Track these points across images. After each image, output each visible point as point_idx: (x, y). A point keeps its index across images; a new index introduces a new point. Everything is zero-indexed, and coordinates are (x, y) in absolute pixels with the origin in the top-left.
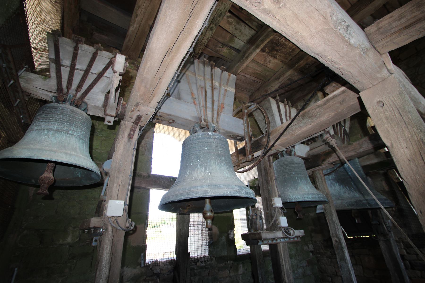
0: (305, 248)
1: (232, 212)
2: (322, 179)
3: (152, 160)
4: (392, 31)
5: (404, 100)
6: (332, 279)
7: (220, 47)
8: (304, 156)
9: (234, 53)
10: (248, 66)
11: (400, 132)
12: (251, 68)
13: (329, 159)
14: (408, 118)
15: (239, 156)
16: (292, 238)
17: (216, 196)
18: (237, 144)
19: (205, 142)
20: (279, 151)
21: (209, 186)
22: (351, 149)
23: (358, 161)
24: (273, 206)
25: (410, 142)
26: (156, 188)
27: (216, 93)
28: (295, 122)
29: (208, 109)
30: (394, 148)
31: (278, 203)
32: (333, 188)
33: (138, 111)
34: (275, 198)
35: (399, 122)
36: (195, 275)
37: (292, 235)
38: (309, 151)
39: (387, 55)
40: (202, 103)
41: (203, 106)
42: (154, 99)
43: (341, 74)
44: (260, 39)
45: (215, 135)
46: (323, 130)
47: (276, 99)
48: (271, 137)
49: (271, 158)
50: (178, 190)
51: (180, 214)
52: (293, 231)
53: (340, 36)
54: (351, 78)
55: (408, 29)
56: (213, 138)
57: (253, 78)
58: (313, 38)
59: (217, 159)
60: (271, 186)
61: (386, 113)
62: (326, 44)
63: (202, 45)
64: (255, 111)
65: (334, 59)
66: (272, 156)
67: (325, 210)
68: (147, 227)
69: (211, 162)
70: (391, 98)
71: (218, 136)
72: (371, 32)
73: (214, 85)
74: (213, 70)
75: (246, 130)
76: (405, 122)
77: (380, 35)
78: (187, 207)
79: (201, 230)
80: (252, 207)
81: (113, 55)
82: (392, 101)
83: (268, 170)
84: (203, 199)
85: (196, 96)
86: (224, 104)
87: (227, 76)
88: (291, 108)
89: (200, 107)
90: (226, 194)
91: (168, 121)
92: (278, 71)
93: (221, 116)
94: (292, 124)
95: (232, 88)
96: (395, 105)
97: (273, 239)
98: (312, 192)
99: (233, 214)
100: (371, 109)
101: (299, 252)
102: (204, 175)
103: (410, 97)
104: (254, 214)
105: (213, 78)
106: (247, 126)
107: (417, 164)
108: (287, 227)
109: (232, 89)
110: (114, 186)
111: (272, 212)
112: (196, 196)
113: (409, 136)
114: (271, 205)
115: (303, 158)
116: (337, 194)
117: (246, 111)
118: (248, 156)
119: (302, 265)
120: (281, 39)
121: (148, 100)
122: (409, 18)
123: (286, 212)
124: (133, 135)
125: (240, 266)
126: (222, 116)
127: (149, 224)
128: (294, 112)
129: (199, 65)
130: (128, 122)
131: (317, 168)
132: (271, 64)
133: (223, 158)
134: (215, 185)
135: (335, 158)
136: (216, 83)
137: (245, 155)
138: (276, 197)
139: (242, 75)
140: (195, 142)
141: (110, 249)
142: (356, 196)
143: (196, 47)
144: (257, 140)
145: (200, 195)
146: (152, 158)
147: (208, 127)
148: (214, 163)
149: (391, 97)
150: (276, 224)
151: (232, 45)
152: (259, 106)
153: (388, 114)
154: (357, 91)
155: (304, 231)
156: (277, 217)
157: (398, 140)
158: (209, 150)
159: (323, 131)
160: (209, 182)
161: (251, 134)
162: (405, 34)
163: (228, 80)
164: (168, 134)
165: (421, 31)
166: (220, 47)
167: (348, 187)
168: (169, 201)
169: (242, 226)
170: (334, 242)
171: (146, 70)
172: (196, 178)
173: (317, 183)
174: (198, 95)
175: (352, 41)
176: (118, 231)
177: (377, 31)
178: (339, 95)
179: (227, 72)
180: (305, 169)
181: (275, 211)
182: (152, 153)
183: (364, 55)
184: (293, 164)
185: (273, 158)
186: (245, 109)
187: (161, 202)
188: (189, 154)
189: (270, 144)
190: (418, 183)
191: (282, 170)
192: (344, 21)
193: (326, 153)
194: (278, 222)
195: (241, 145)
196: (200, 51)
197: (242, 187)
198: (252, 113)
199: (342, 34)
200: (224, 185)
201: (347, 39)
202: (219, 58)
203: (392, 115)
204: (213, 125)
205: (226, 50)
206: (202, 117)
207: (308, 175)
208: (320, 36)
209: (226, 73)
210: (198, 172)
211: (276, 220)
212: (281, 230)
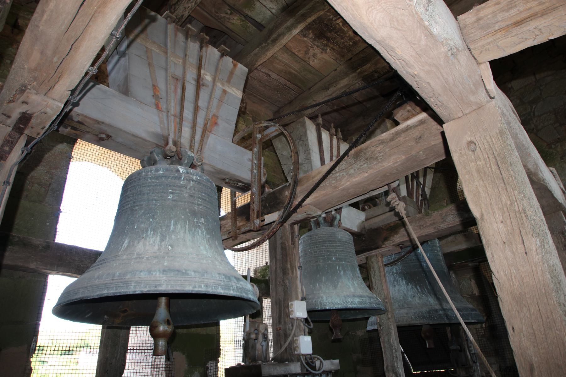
1: (218, 325)
2: (380, 272)
3: (59, 214)
4: (497, 27)
5: (505, 144)
7: (227, 13)
8: (355, 229)
9: (252, 28)
10: (275, 58)
11: (495, 195)
12: (280, 61)
13: (394, 237)
14: (509, 173)
15: (239, 219)
16: (318, 374)
17: (177, 292)
18: (235, 196)
19: (170, 186)
22: (428, 224)
23: (438, 245)
24: (291, 316)
25: (508, 214)
26: (62, 273)
27: (204, 94)
28: (343, 165)
29: (183, 122)
30: (485, 220)
32: (397, 287)
33: (23, 103)
35: (495, 179)
37: (317, 369)
38: (363, 222)
39: (487, 66)
40: (172, 109)
41: (175, 116)
42: (60, 82)
43: (417, 86)
44: (300, 12)
45: (191, 174)
46: (387, 185)
47: (316, 121)
48: (299, 189)
49: (296, 227)
50: (98, 278)
51: (108, 328)
52: (321, 362)
53: (416, 16)
54: (431, 96)
55: (519, 27)
56: (187, 180)
57: (282, 81)
58: (373, 9)
59: (189, 220)
61: (479, 163)
62: (392, 26)
64: (277, 139)
65: (406, 57)
66: (299, 224)
67: (380, 326)
68: (34, 353)
69: (175, 225)
70: (488, 139)
71: (197, 176)
72: (467, 23)
73: (203, 79)
74: (204, 49)
76: (503, 180)
77: (480, 31)
79: (150, 360)
80: (250, 317)
82: (488, 143)
83: (288, 248)
84: (155, 297)
85: (163, 94)
86: (218, 117)
87: (231, 65)
88: (341, 142)
89: (167, 116)
91: (97, 136)
92: (328, 76)
93: (210, 139)
94: (337, 169)
95: (238, 89)
96: (493, 151)
98: (361, 293)
99: (219, 331)
100: (457, 154)
102: (159, 249)
103: (515, 143)
104: (253, 330)
105: (203, 64)
106: (259, 164)
107: (514, 250)
108: (310, 354)
109: (236, 92)
111: (288, 328)
112: (133, 290)
113: (506, 204)
114: (287, 314)
115: (353, 234)
116: (402, 298)
117: (259, 136)
118: (253, 221)
120: (336, 20)
121: (48, 81)
122: (521, 9)
123: (312, 327)
124: (9, 154)
126: (211, 140)
127: (38, 345)
128: (344, 147)
129: (176, 35)
131: (374, 252)
132: (316, 61)
134: (178, 271)
135: (404, 235)
136: (206, 75)
137: (248, 219)
138: (297, 299)
139: (263, 72)
140: (149, 183)
142: (430, 302)
143: (179, 3)
144: (274, 193)
145: (142, 289)
146: (60, 209)
147: (180, 157)
148: (181, 227)
149: (488, 137)
150: (291, 349)
151: (249, 14)
152: (283, 130)
153: (480, 163)
154: (440, 122)
155: (340, 361)
156: (295, 335)
157: (491, 208)
158: (174, 200)
160: (166, 264)
161: (263, 179)
162: (513, 34)
163: (232, 73)
164: (104, 165)
165: (537, 34)
166: (227, 13)
167: (420, 287)
169: (236, 353)
171: (45, 16)
172: (141, 255)
173: (372, 279)
174: (167, 92)
175: (435, 30)
177: (475, 22)
178: (415, 126)
179: (231, 59)
180: (354, 252)
181: (292, 326)
182: (61, 200)
183: (452, 57)
184: (335, 241)
185: (301, 228)
187: (60, 299)
188: (134, 207)
189: (296, 203)
190: (514, 281)
193: (391, 226)
194: (295, 345)
195: (243, 200)
196: (187, 12)
197: (233, 276)
198: (270, 140)
199: (419, 13)
200: (195, 272)
201: (427, 23)
202: (223, 33)
203: (487, 167)
204: (190, 153)
205: (238, 19)
206: (169, 135)
207: (357, 264)
208: (384, 10)
209: (228, 60)
210: (147, 243)
211: (293, 342)
212: (299, 360)
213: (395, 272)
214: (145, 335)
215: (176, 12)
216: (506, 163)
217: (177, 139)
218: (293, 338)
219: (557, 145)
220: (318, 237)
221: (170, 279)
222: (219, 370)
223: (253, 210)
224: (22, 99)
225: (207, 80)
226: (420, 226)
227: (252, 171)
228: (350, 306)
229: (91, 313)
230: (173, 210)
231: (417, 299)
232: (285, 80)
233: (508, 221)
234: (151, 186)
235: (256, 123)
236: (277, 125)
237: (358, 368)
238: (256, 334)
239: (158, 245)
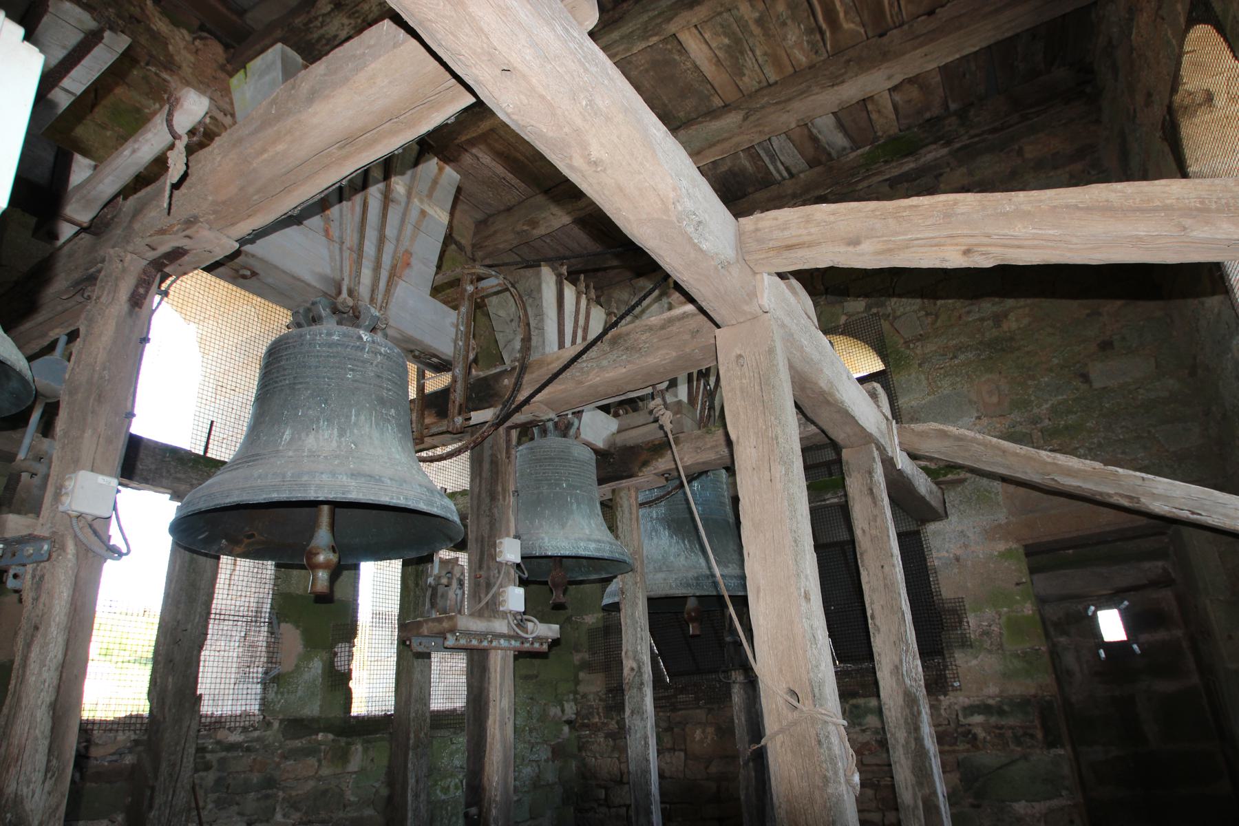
0: (554, 711)
2: (631, 513)
6: (606, 794)
8: (600, 444)
12: (501, 137)
17: (371, 502)
19: (349, 359)
20: (538, 419)
21: (352, 475)
23: (724, 480)
24: (498, 559)
28: (593, 352)
31: (510, 551)
32: (655, 540)
34: (507, 539)
36: (208, 767)
38: (614, 434)
41: (350, 249)
45: (378, 344)
49: (514, 434)
50: (259, 477)
56: (372, 352)
59: (376, 410)
60: (500, 506)
61: (744, 381)
63: (358, 17)
66: (518, 430)
71: (385, 347)
75: (461, 343)
78: (245, 540)
81: (95, 20)
82: (756, 359)
86: (411, 254)
87: (436, 168)
89: (341, 250)
90: (394, 501)
94: (584, 357)
97: (482, 636)
101: (534, 721)
104: (444, 573)
109: (441, 214)
110: (86, 435)
112: (315, 495)
115: (597, 451)
116: (660, 557)
117: (470, 288)
119: (534, 757)
124: (145, 298)
125: (356, 749)
126: (402, 290)
130: (135, 256)
131: (624, 483)
133: (393, 411)
134: (370, 476)
136: (398, 184)
138: (508, 535)
140: (318, 351)
141: (70, 599)
142: (700, 564)
143: (332, 14)
144: (485, 379)
145: (326, 495)
147: (357, 314)
148: (366, 419)
149: (757, 354)
156: (501, 586)
158: (356, 381)
159: (651, 388)
160: (352, 466)
163: (435, 182)
167: (689, 541)
168: (230, 503)
170: (626, 671)
172: (314, 452)
176: (90, 555)
180: (595, 478)
181: (499, 572)
183: (722, 270)
186: (468, 282)
188: (294, 384)
189: (521, 397)
191: (536, 474)
192: (695, 214)
193: (654, 445)
194: (501, 599)
195: (436, 383)
201: (696, 241)
206: (343, 279)
210: (321, 437)
213: (655, 517)
214: (225, 596)
215: (325, 28)
216: (769, 385)
217: (352, 286)
218: (499, 588)
219: (917, 344)
220: (544, 451)
221: (362, 485)
222: (354, 657)
223: (454, 402)
224: (187, 233)
225: (399, 193)
226: (697, 448)
227: (455, 342)
228: (582, 553)
229: (207, 533)
230: (353, 394)
231: (682, 558)
233: (761, 448)
234: (321, 356)
235: (466, 267)
236: (501, 277)
237: (582, 675)
238: (449, 578)
239: (337, 441)
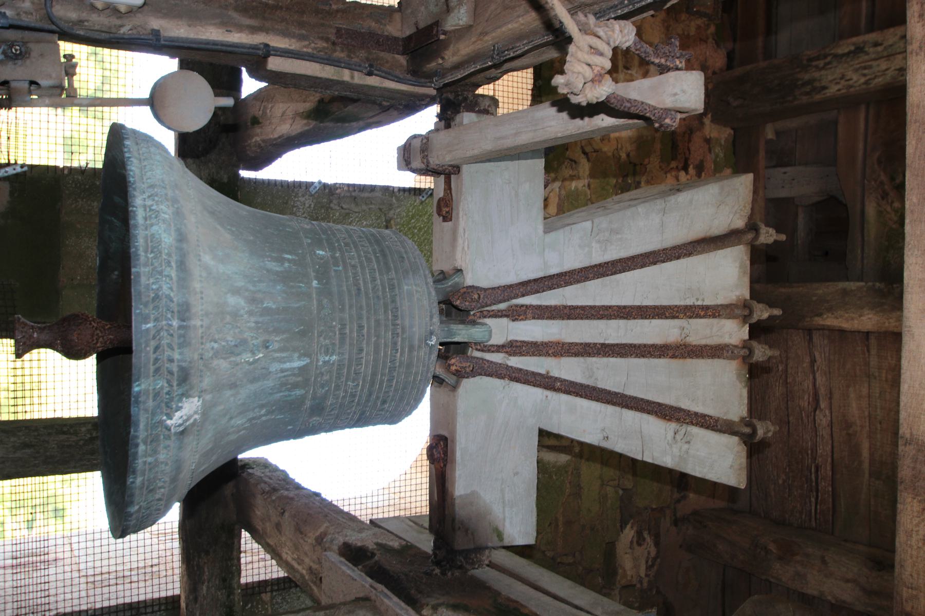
63: (865, 75)
232: (830, 454)
